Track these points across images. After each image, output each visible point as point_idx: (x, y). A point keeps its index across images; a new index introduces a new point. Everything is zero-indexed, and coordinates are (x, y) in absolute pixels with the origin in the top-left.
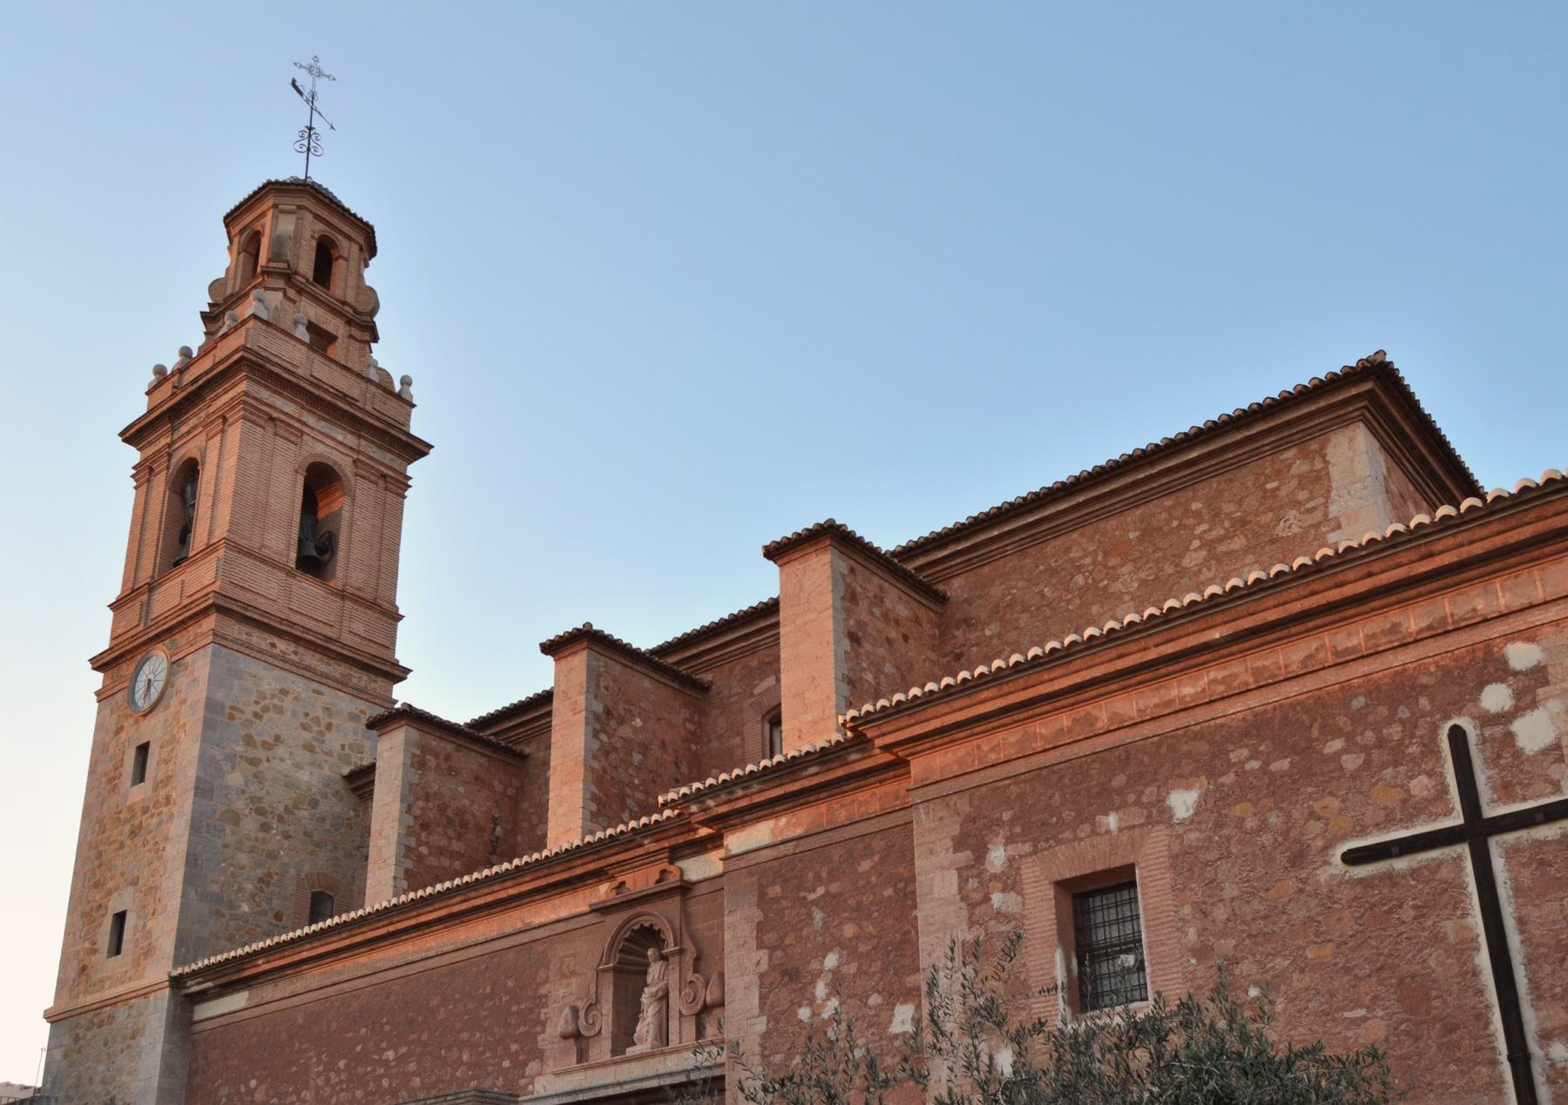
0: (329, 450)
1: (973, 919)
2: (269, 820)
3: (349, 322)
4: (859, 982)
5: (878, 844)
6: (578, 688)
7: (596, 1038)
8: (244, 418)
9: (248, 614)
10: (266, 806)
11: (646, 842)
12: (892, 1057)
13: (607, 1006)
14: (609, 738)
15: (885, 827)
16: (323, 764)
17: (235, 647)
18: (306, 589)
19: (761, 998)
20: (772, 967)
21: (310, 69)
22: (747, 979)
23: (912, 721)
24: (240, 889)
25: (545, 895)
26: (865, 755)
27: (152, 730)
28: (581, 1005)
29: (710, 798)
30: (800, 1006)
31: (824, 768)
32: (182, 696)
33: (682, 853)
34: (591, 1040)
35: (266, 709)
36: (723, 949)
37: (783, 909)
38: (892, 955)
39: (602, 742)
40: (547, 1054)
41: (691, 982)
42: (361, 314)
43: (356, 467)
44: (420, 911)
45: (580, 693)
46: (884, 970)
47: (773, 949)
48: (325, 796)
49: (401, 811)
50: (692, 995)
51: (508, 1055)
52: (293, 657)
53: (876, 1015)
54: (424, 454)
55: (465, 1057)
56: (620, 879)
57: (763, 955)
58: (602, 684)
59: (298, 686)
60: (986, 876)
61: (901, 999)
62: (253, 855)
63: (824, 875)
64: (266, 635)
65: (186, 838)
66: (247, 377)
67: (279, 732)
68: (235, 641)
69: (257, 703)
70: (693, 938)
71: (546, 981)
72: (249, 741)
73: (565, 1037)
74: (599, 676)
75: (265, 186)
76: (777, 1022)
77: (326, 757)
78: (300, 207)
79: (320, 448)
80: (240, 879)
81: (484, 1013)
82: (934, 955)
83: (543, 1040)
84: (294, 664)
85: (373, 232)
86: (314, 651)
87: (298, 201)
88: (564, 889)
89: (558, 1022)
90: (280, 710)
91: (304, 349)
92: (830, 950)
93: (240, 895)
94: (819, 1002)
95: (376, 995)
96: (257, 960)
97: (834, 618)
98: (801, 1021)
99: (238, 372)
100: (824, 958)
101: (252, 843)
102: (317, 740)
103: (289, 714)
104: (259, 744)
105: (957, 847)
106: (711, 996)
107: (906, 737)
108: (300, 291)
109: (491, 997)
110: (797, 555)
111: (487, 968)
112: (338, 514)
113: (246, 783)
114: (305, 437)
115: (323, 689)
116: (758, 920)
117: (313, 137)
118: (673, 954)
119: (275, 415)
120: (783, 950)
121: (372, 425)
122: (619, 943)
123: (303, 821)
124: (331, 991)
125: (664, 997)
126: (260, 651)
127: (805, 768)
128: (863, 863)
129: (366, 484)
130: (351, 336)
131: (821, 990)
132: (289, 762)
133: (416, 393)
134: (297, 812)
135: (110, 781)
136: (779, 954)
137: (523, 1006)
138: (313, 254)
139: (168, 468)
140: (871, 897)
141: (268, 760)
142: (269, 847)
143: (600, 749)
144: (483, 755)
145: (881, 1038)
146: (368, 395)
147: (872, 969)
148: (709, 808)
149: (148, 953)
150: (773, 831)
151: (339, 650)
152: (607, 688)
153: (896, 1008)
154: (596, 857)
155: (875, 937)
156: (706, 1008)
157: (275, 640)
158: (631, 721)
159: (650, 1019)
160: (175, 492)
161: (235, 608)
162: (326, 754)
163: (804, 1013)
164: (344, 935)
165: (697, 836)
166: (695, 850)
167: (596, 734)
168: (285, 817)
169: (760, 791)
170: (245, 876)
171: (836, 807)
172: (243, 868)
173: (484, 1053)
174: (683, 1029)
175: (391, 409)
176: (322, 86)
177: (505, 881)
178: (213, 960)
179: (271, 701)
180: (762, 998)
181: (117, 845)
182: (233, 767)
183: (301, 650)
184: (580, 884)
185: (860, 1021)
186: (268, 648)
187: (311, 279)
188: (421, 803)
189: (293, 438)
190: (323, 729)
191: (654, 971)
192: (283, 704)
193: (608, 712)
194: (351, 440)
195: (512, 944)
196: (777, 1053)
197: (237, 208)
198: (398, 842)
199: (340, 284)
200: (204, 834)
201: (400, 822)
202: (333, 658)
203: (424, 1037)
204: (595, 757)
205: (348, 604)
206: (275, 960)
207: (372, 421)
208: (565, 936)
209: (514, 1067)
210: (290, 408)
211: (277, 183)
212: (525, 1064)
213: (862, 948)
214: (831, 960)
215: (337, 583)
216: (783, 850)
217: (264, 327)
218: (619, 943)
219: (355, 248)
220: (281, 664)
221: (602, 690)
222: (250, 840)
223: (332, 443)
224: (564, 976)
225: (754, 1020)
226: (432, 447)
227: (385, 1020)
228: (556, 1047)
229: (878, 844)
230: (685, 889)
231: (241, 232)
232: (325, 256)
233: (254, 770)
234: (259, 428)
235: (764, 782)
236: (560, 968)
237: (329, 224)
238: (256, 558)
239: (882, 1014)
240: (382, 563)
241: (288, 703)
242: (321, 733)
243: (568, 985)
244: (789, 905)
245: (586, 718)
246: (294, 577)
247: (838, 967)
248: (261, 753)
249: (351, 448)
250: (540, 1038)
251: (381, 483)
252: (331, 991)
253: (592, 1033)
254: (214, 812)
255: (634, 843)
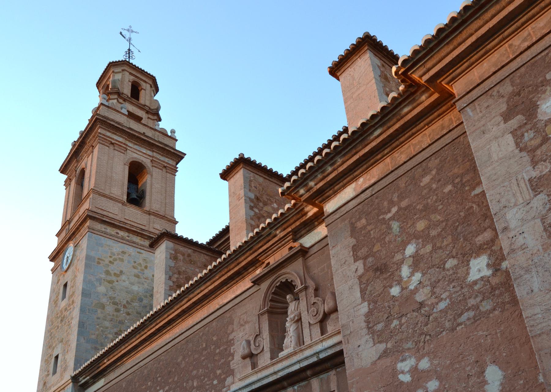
0: (140, 156)
1: (536, 159)
2: (119, 307)
3: (147, 112)
4: (434, 255)
5: (434, 163)
6: (240, 188)
7: (261, 354)
8: (99, 143)
9: (104, 219)
10: (117, 301)
11: (278, 232)
12: (475, 298)
13: (266, 334)
14: (259, 211)
15: (437, 149)
16: (144, 283)
17: (99, 233)
18: (131, 210)
19: (361, 291)
20: (366, 270)
21: (128, 30)
22: (350, 283)
23: (451, 47)
24: (106, 337)
25: (228, 286)
26: (415, 104)
27: (68, 277)
28: (251, 339)
29: (311, 181)
30: (391, 287)
31: (385, 127)
32: (78, 258)
33: (300, 234)
34: (259, 355)
35: (115, 260)
36: (332, 279)
37: (369, 231)
38: (459, 228)
39: (255, 212)
40: (236, 371)
41: (314, 303)
42: (153, 110)
43: (152, 163)
44: (169, 313)
45: (241, 189)
46: (455, 240)
47: (365, 258)
48: (146, 297)
49: (166, 279)
50: (316, 310)
51: (216, 377)
52: (127, 238)
53: (454, 273)
54: (182, 158)
55: (195, 385)
56: (266, 262)
57: (360, 265)
58: (253, 185)
59: (131, 250)
60: (540, 125)
61: (474, 255)
62: (112, 322)
63: (395, 199)
64: (114, 229)
65: (78, 316)
66: (100, 127)
67: (122, 269)
68: (99, 231)
69: (110, 257)
70: (313, 279)
71: (233, 331)
72: (108, 273)
73: (244, 358)
74: (251, 181)
75: (109, 65)
76: (375, 302)
77: (146, 280)
78: (123, 70)
79: (135, 155)
80: (106, 333)
81: (203, 358)
82: (503, 200)
83: (233, 364)
84: (128, 241)
85: (156, 80)
86: (137, 236)
87: (123, 68)
88: (237, 279)
89: (240, 349)
90: (122, 260)
91: (126, 117)
92: (409, 243)
93: (106, 340)
94: (405, 279)
95: (154, 364)
96: (104, 360)
97: (376, 83)
98: (393, 296)
99: (96, 126)
100: (405, 250)
101: (112, 317)
102: (141, 273)
103: (126, 262)
104: (113, 274)
105: (507, 117)
106: (327, 307)
107: (448, 62)
108: (125, 100)
109: (205, 349)
110: (348, 65)
111: (203, 334)
112: (146, 182)
113: (107, 291)
114: (128, 151)
115: (142, 251)
116: (352, 244)
117: (131, 53)
118: (301, 291)
119: (113, 142)
120: (373, 256)
121: (158, 146)
122: (269, 296)
123: (136, 308)
124: (135, 368)
125: (299, 320)
126: (111, 235)
127: (372, 133)
128: (424, 179)
129: (157, 170)
130: (148, 118)
131: (405, 271)
132: (127, 282)
133: (177, 135)
134: (132, 303)
135: (55, 303)
136: (370, 259)
137: (221, 348)
138: (130, 87)
139: (75, 176)
140: (435, 197)
141: (117, 281)
142: (120, 319)
143: (254, 215)
144: (208, 255)
145: (462, 288)
146: (156, 136)
147: (445, 243)
148: (311, 188)
149: (65, 370)
150: (355, 190)
151: (148, 234)
152: (256, 187)
153: (471, 263)
154: (251, 251)
155: (442, 222)
156: (326, 316)
157: (118, 231)
158: (271, 204)
159: (291, 334)
160: (79, 184)
161: (97, 217)
162: (145, 279)
163: (395, 291)
164: (137, 337)
165: (308, 217)
166: (307, 229)
167: (251, 208)
168: (127, 305)
169: (343, 163)
170: (109, 332)
171: (397, 155)
172: (107, 328)
173: (204, 379)
174: (312, 333)
175: (167, 141)
176: (133, 35)
177: (206, 282)
178: (86, 364)
179: (117, 256)
180: (363, 292)
181: (56, 328)
182: (100, 284)
183: (131, 235)
184: (246, 273)
185: (441, 282)
186: (115, 234)
187: (130, 96)
188: (176, 276)
189: (123, 151)
190: (143, 268)
191: (292, 307)
192: (123, 258)
193: (257, 199)
194: (149, 153)
195: (214, 317)
196: (379, 323)
197: (100, 78)
198: (165, 293)
199: (144, 98)
200: (87, 313)
201: (165, 283)
202: (146, 239)
203: (176, 379)
204: (252, 219)
205: (152, 217)
206: (112, 358)
207: (157, 144)
208: (240, 304)
209: (219, 383)
210: (121, 139)
211: (113, 62)
212: (225, 379)
213: (433, 233)
214: (410, 250)
215: (147, 207)
216: (363, 196)
217: (107, 108)
218: (269, 296)
219: (148, 86)
220: (121, 241)
221: (253, 188)
222: (110, 316)
223: (140, 154)
224: (242, 325)
225: (359, 307)
226: (185, 154)
227: (158, 375)
228: (240, 365)
229: (434, 163)
230: (304, 252)
231: (102, 88)
232: (136, 91)
233: (111, 285)
234: (106, 147)
235: (344, 155)
236: (239, 322)
237: (136, 77)
238: (107, 197)
239: (460, 271)
240: (167, 201)
241: (126, 257)
242: (142, 270)
243: (244, 330)
244: (374, 227)
245: (245, 200)
246: (126, 205)
247: (417, 251)
248: (114, 278)
249: (149, 156)
250: (231, 363)
251: (164, 170)
252: (135, 368)
253: (259, 351)
254: (92, 303)
255: (271, 236)
